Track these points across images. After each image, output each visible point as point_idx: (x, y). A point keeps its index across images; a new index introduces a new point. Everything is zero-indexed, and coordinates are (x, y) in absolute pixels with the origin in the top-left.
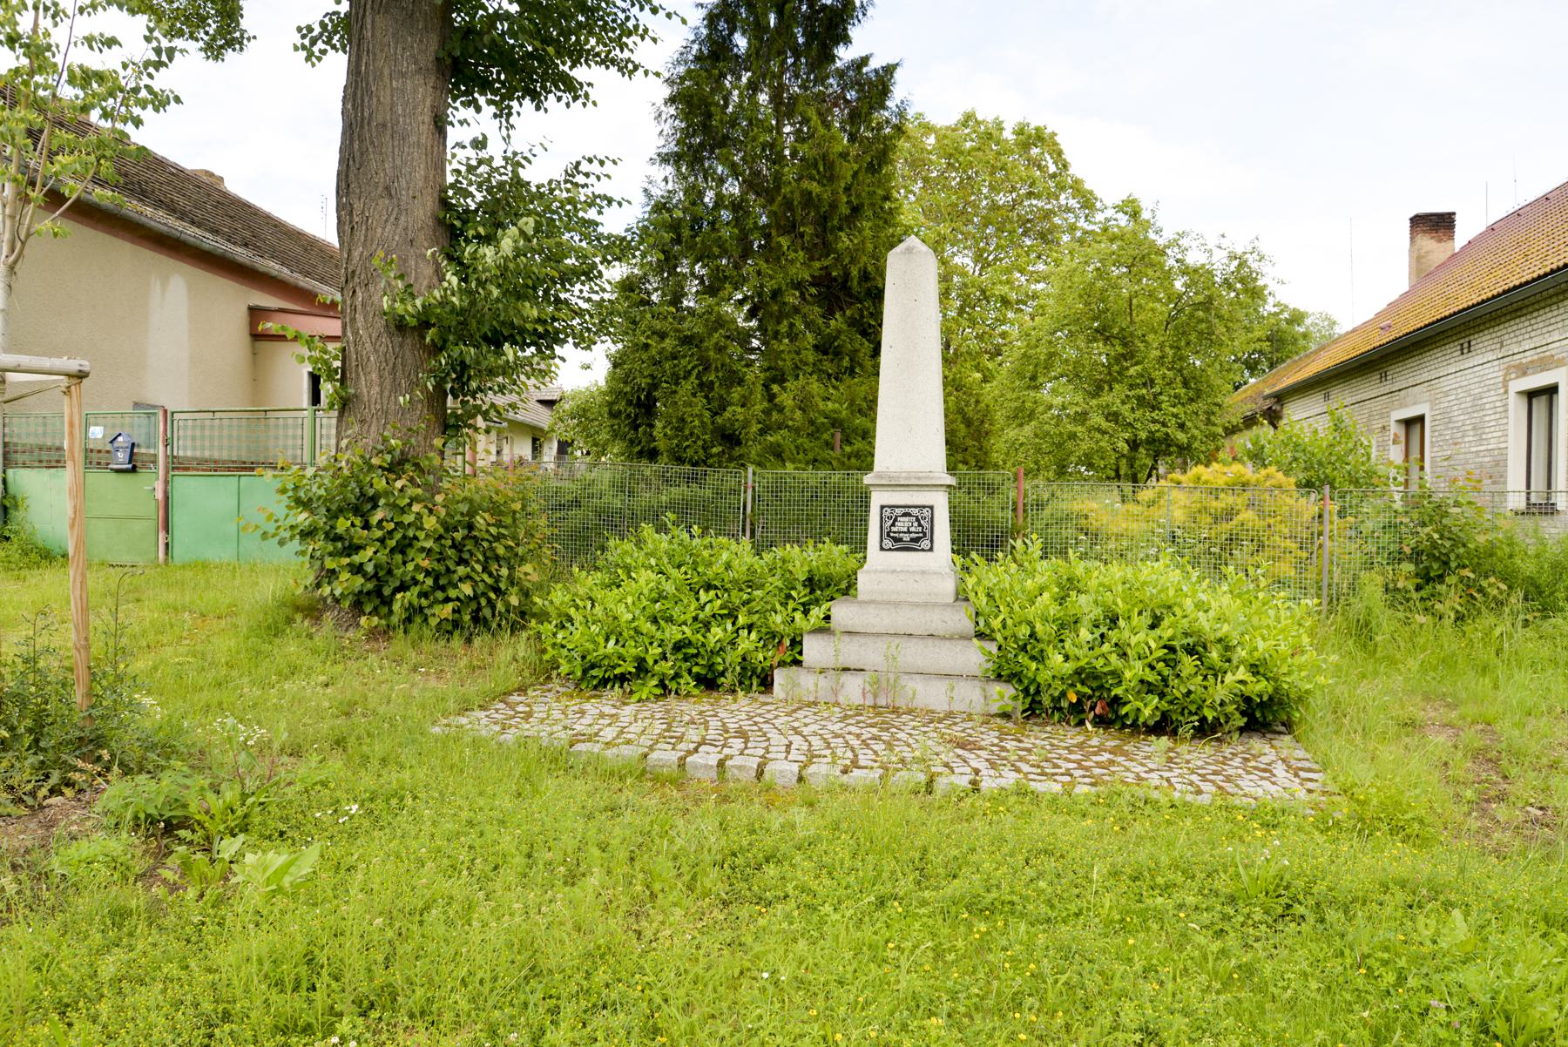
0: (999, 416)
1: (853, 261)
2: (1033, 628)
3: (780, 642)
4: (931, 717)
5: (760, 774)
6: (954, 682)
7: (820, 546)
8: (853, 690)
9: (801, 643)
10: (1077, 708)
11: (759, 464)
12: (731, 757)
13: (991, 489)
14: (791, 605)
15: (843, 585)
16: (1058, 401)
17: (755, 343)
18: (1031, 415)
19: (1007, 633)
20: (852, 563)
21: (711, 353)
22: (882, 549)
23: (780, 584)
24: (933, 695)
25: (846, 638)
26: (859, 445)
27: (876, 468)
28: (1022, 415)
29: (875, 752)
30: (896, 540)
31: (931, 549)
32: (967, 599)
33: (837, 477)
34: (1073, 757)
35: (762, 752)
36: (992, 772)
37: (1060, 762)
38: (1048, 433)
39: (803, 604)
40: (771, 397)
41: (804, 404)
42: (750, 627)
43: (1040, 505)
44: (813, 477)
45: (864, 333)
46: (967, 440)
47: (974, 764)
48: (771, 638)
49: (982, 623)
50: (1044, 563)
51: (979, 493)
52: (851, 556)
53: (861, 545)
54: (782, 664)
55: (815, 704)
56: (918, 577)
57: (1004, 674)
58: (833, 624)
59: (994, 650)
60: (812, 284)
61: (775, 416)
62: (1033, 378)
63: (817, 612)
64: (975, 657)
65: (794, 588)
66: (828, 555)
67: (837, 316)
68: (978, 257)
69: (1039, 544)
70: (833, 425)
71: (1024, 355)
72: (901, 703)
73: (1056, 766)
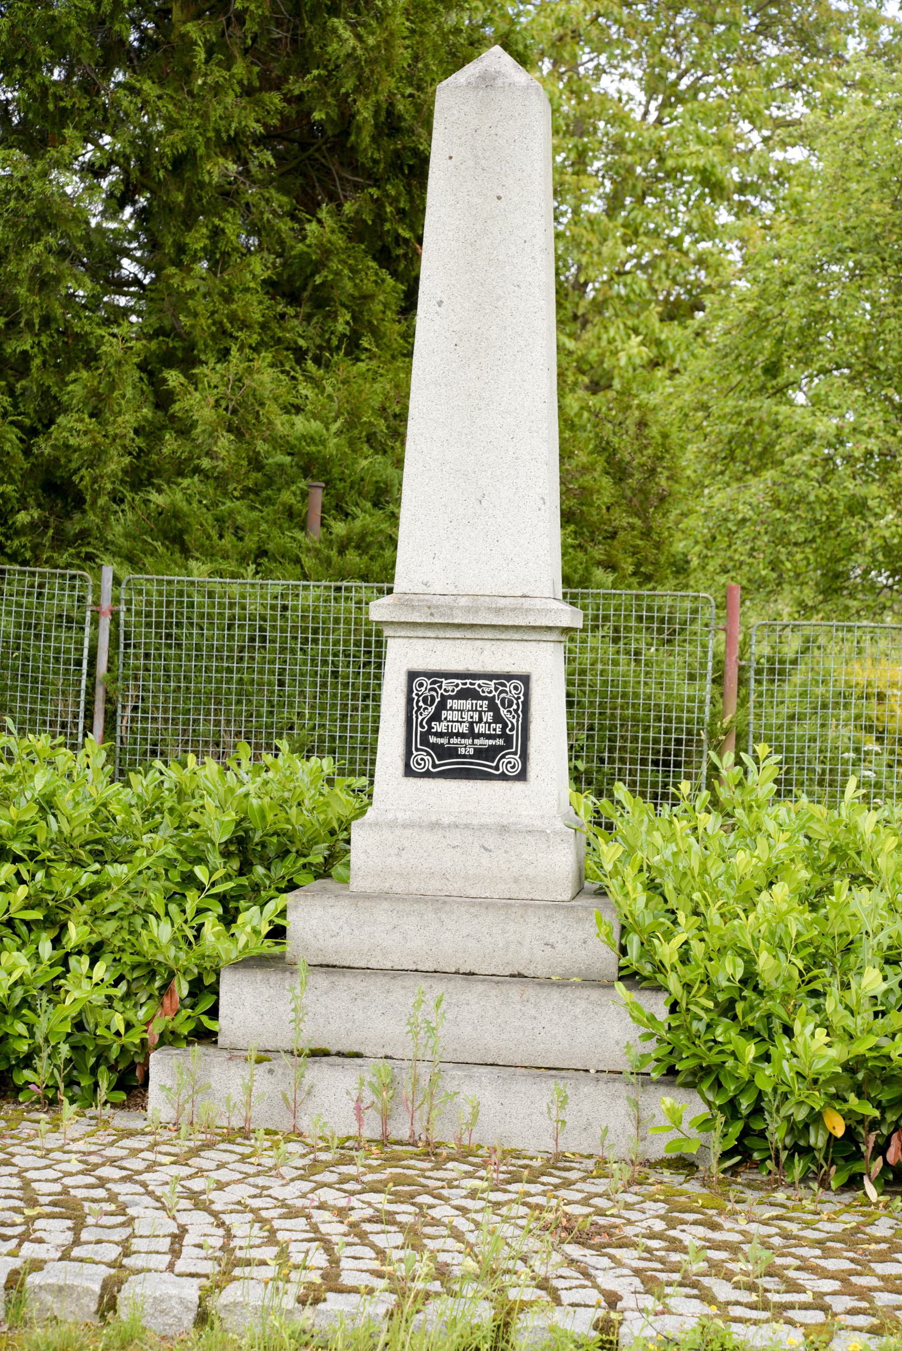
0: (690, 460)
1: (363, 86)
2: (750, 962)
3: (166, 988)
4: (516, 1167)
5: (108, 1304)
6: (567, 1085)
7: (267, 758)
8: (334, 1101)
9: (214, 990)
10: (846, 1148)
11: (131, 560)
12: (37, 1265)
13: (669, 631)
14: (193, 900)
15: (316, 858)
16: (826, 425)
17: (129, 267)
18: (766, 457)
19: (692, 974)
20: (341, 802)
21: (21, 291)
22: (409, 772)
23: (169, 850)
24: (518, 1117)
25: (321, 980)
26: (365, 519)
27: (400, 584)
28: (749, 451)
29: (381, 1254)
30: (443, 752)
31: (522, 776)
32: (602, 893)
33: (312, 594)
34: (832, 1264)
35: (112, 1252)
36: (649, 1302)
37: (802, 1277)
38: (802, 498)
39: (223, 899)
40: (163, 400)
41: (240, 419)
42: (95, 952)
43: (777, 670)
44: (256, 592)
45: (384, 257)
46: (612, 518)
47: (607, 1281)
48: (145, 976)
49: (634, 950)
50: (782, 810)
51: (639, 640)
52: (342, 782)
53: (360, 761)
54: (169, 1038)
55: (245, 1133)
56: (491, 841)
57: (680, 1068)
58: (290, 947)
59: (662, 1013)
60: (261, 141)
61: (170, 444)
62: (772, 369)
63: (253, 920)
64: (617, 1027)
65: (201, 860)
66: (284, 782)
67: (323, 214)
68: (653, 85)
69: (771, 767)
70: (306, 472)
71: (754, 315)
72: (444, 1133)
73: (794, 1287)
